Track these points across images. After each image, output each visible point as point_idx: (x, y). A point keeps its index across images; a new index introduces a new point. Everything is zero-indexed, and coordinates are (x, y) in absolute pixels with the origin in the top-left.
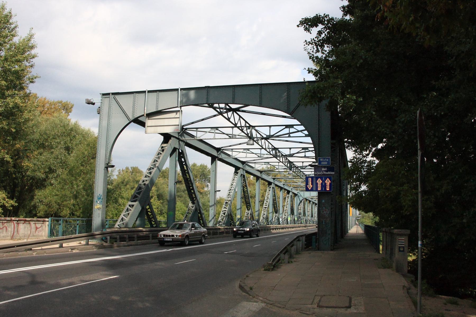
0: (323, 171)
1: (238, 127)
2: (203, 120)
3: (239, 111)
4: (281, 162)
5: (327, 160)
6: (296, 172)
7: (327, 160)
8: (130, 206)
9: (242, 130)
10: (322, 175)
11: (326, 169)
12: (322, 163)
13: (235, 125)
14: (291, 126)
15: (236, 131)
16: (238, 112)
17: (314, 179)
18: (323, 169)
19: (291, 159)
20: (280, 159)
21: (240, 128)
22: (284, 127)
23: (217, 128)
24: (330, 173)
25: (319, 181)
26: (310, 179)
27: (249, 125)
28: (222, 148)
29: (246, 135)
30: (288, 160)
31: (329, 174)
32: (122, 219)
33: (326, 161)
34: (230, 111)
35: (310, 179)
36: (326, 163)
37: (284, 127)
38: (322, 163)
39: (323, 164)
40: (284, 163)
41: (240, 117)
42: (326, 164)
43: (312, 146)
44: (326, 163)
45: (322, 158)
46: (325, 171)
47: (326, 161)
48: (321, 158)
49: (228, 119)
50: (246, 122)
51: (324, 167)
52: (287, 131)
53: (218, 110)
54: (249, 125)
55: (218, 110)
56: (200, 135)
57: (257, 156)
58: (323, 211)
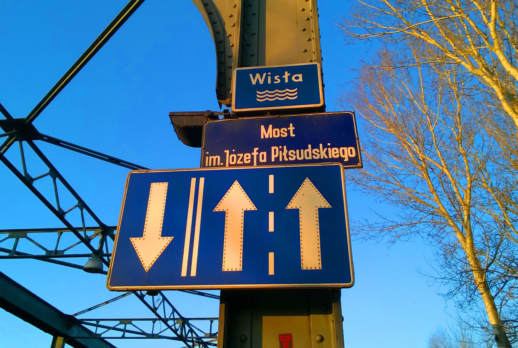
12: (261, 96)
23: (129, 321)
27: (179, 317)
33: (291, 85)
36: (292, 94)
38: (261, 96)
44: (292, 94)
46: (278, 142)
47: (291, 85)
48: (254, 72)
50: (174, 310)
54: (179, 317)
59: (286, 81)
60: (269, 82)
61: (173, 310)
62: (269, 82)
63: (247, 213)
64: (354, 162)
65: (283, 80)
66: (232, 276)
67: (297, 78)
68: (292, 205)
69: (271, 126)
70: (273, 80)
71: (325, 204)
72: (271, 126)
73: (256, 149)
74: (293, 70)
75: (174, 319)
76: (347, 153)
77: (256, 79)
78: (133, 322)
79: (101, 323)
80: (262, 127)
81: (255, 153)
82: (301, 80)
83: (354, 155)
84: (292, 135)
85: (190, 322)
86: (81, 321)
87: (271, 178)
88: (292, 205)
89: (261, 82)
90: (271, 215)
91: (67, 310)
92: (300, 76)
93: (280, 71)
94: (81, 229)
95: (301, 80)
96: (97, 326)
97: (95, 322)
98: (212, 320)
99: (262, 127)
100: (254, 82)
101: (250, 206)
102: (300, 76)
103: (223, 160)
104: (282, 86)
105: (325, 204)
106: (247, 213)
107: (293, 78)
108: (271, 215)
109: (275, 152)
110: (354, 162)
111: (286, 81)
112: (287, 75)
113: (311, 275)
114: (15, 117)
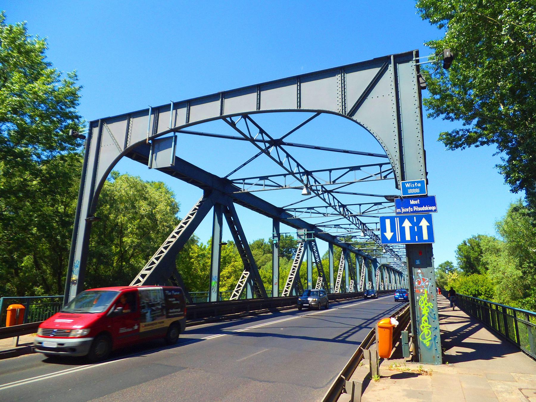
0: (412, 206)
1: (332, 207)
2: (245, 164)
3: (333, 192)
4: (353, 224)
5: (419, 185)
6: (356, 224)
7: (419, 185)
8: (245, 274)
9: (336, 209)
10: (411, 212)
11: (417, 202)
13: (330, 205)
14: (380, 204)
15: (330, 210)
16: (332, 193)
17: (397, 220)
18: (412, 202)
19: (363, 220)
20: (349, 219)
21: (334, 207)
22: (373, 204)
23: (312, 208)
24: (426, 208)
25: (407, 224)
26: (388, 222)
27: (304, 171)
28: (284, 207)
29: (338, 213)
30: (359, 221)
31: (425, 211)
32: (339, 275)
33: (417, 187)
34: (325, 192)
35: (388, 222)
37: (373, 204)
38: (410, 191)
39: (411, 194)
40: (370, 236)
41: (334, 197)
42: (417, 193)
43: (405, 249)
44: (417, 190)
45: (409, 183)
46: (415, 205)
47: (417, 187)
48: (407, 183)
49: (324, 200)
51: (415, 198)
52: (376, 207)
53: (316, 192)
54: (304, 171)
55: (316, 192)
56: (247, 188)
57: (347, 231)
58: (419, 283)
59: (416, 186)
60: (411, 186)
61: (297, 165)
62: (411, 186)
63: (410, 227)
64: (435, 211)
65: (415, 185)
66: (408, 241)
67: (419, 185)
68: (420, 225)
69: (413, 200)
70: (412, 186)
71: (429, 225)
72: (413, 200)
73: (409, 207)
74: (418, 182)
75: (299, 173)
76: (433, 208)
77: (408, 185)
78: (269, 178)
79: (246, 181)
80: (410, 200)
81: (409, 208)
82: (420, 186)
83: (435, 209)
84: (419, 203)
85: (313, 173)
86: (232, 181)
87: (415, 217)
88: (420, 225)
89: (409, 186)
90: (416, 227)
91: (278, 205)
92: (420, 184)
93: (414, 183)
94: (334, 206)
95: (420, 186)
96: (324, 226)
97: (242, 181)
98: (376, 223)
99: (410, 200)
100: (407, 187)
101: (411, 225)
102: (420, 184)
103: (401, 210)
104: (415, 188)
105: (429, 225)
106: (410, 227)
107: (418, 185)
108: (416, 227)
109: (415, 208)
110: (435, 211)
111: (416, 186)
112: (416, 184)
113: (425, 241)
114: (274, 138)
